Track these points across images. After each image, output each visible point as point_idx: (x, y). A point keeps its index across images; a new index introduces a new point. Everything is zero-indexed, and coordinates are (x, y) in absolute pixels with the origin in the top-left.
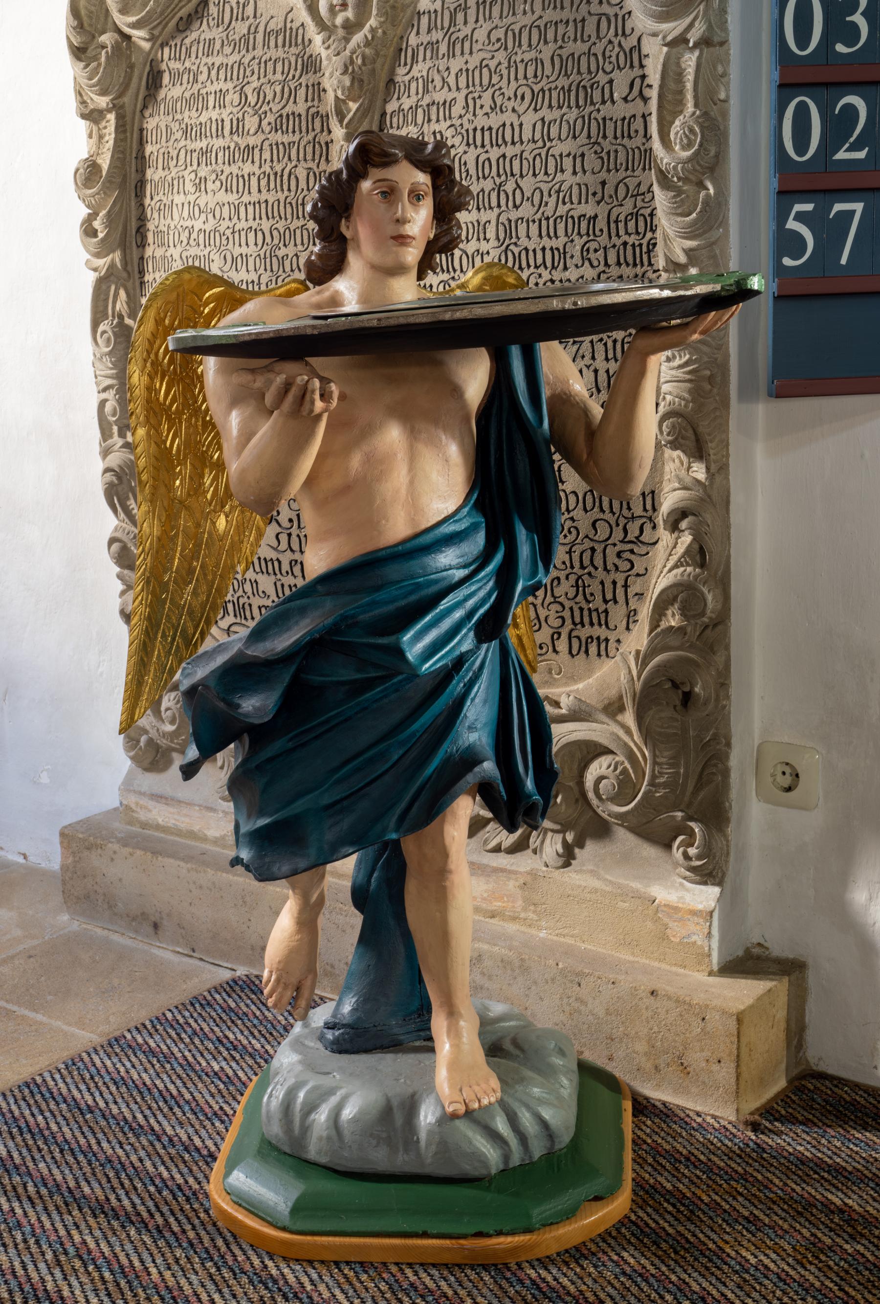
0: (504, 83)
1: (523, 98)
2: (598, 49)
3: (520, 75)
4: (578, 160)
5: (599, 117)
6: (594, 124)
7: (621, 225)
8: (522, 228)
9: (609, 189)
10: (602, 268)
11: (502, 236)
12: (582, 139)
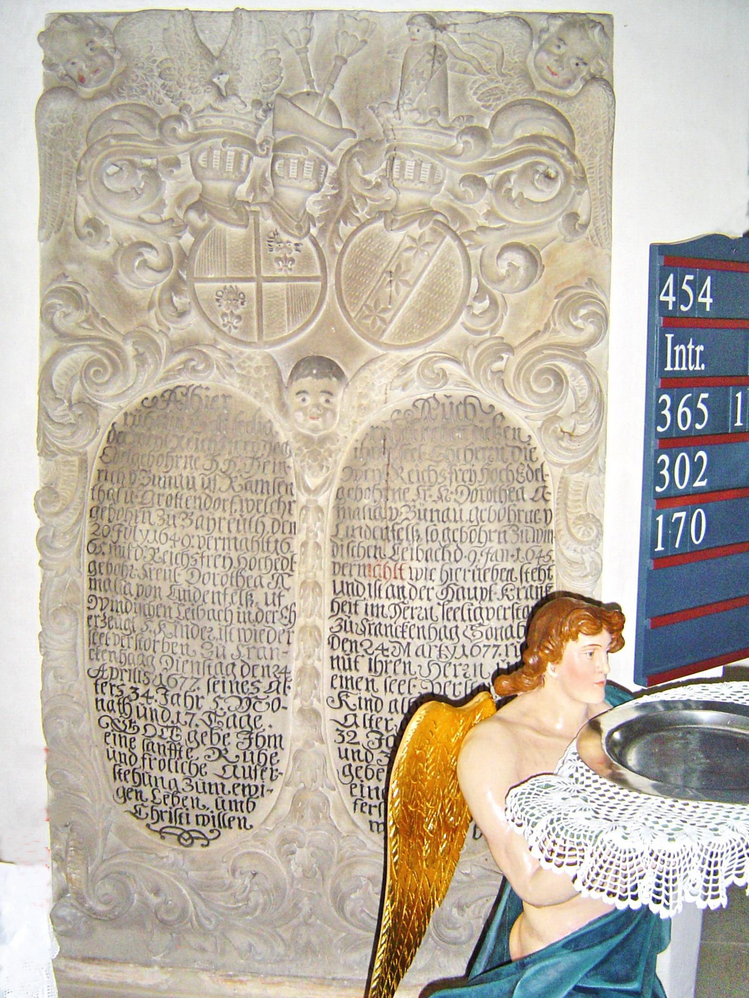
0: (447, 482)
1: (462, 492)
2: (514, 467)
3: (460, 478)
4: (502, 535)
5: (516, 509)
6: (512, 513)
7: (529, 576)
8: (460, 575)
9: (522, 554)
10: (515, 600)
11: (444, 578)
12: (505, 522)
